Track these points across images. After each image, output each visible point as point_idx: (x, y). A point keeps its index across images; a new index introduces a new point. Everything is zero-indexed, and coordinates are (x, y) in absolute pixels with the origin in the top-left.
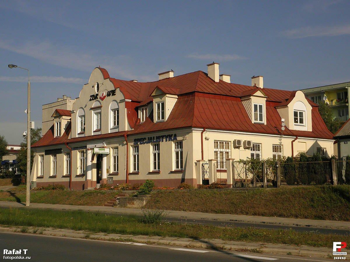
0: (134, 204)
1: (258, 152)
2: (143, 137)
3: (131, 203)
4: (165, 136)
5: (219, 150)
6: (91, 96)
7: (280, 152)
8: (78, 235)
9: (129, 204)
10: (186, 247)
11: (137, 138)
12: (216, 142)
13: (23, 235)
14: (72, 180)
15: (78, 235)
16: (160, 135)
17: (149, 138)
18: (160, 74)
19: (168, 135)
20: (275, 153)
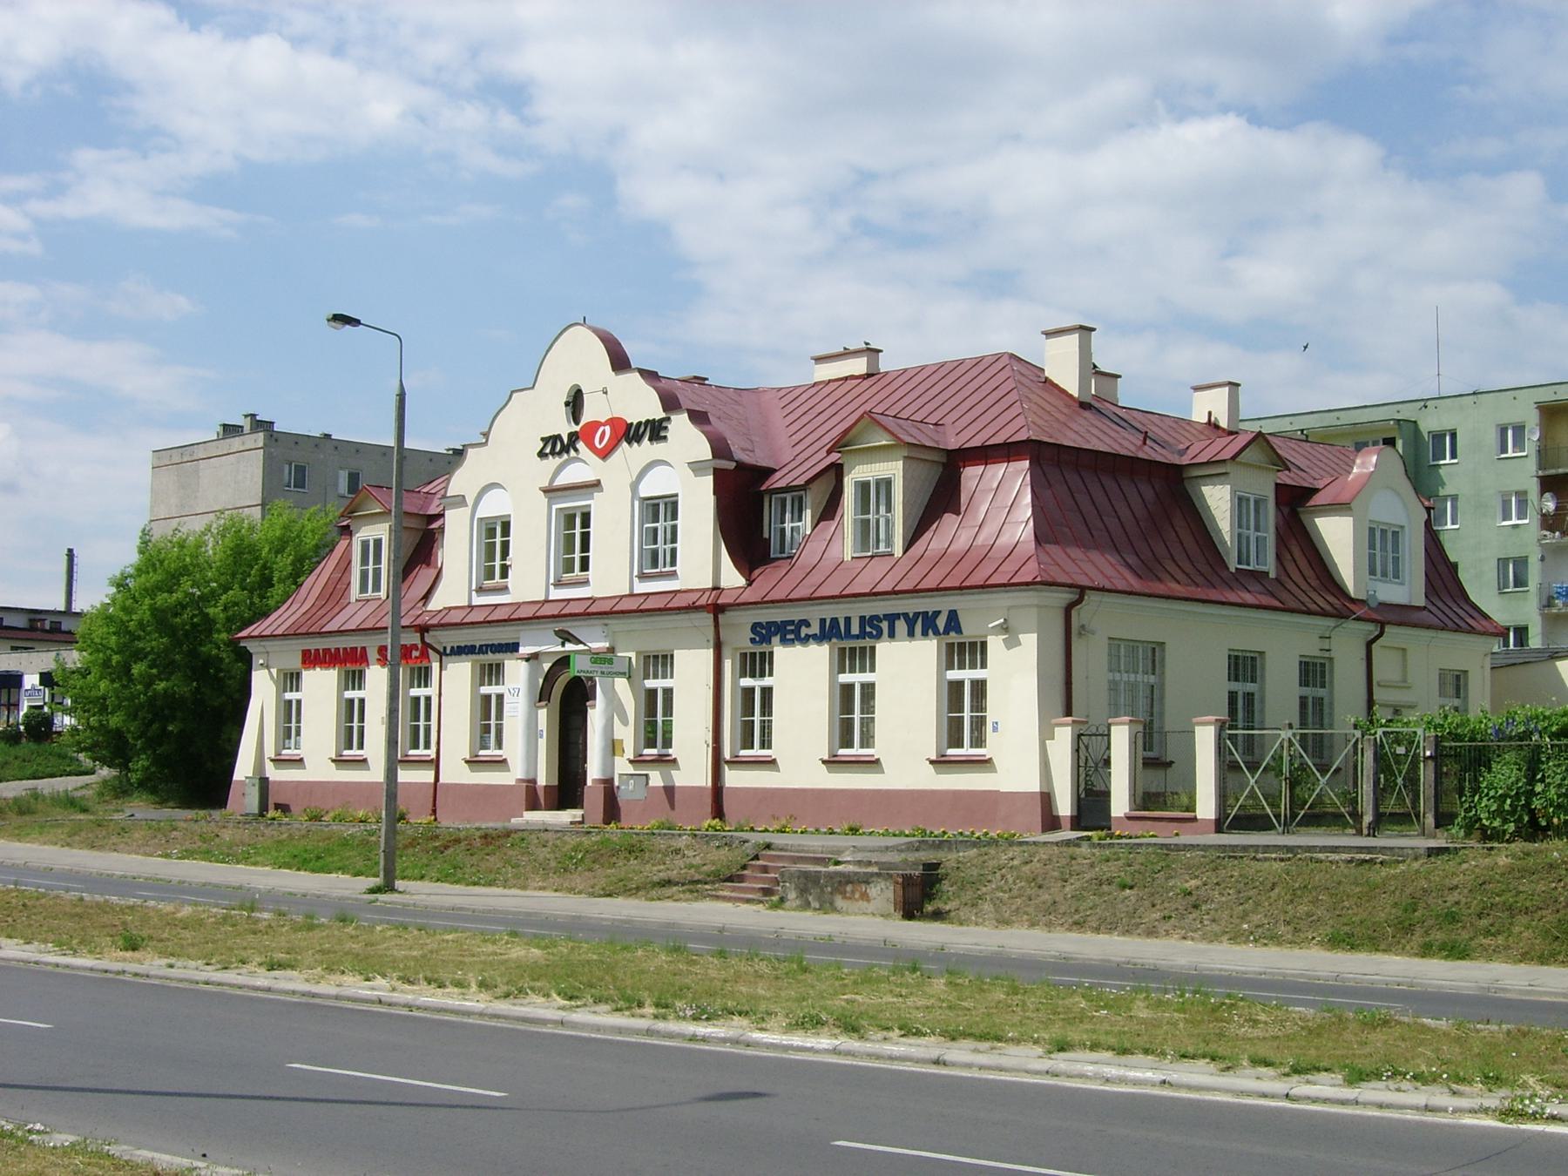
0: (868, 900)
1: (1251, 687)
2: (796, 618)
3: (853, 892)
4: (906, 615)
5: (1139, 677)
6: (545, 440)
7: (1323, 686)
8: (1469, 1110)
9: (845, 898)
10: (1380, 1106)
11: (763, 620)
12: (755, 627)
13: (1240, 1105)
14: (442, 780)
15: (1469, 1110)
16: (881, 612)
17: (823, 621)
18: (819, 360)
19: (917, 615)
20: (1235, 686)
